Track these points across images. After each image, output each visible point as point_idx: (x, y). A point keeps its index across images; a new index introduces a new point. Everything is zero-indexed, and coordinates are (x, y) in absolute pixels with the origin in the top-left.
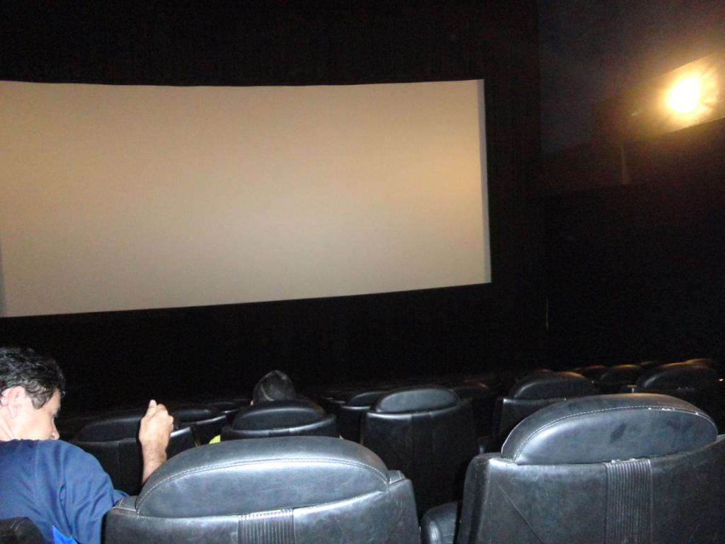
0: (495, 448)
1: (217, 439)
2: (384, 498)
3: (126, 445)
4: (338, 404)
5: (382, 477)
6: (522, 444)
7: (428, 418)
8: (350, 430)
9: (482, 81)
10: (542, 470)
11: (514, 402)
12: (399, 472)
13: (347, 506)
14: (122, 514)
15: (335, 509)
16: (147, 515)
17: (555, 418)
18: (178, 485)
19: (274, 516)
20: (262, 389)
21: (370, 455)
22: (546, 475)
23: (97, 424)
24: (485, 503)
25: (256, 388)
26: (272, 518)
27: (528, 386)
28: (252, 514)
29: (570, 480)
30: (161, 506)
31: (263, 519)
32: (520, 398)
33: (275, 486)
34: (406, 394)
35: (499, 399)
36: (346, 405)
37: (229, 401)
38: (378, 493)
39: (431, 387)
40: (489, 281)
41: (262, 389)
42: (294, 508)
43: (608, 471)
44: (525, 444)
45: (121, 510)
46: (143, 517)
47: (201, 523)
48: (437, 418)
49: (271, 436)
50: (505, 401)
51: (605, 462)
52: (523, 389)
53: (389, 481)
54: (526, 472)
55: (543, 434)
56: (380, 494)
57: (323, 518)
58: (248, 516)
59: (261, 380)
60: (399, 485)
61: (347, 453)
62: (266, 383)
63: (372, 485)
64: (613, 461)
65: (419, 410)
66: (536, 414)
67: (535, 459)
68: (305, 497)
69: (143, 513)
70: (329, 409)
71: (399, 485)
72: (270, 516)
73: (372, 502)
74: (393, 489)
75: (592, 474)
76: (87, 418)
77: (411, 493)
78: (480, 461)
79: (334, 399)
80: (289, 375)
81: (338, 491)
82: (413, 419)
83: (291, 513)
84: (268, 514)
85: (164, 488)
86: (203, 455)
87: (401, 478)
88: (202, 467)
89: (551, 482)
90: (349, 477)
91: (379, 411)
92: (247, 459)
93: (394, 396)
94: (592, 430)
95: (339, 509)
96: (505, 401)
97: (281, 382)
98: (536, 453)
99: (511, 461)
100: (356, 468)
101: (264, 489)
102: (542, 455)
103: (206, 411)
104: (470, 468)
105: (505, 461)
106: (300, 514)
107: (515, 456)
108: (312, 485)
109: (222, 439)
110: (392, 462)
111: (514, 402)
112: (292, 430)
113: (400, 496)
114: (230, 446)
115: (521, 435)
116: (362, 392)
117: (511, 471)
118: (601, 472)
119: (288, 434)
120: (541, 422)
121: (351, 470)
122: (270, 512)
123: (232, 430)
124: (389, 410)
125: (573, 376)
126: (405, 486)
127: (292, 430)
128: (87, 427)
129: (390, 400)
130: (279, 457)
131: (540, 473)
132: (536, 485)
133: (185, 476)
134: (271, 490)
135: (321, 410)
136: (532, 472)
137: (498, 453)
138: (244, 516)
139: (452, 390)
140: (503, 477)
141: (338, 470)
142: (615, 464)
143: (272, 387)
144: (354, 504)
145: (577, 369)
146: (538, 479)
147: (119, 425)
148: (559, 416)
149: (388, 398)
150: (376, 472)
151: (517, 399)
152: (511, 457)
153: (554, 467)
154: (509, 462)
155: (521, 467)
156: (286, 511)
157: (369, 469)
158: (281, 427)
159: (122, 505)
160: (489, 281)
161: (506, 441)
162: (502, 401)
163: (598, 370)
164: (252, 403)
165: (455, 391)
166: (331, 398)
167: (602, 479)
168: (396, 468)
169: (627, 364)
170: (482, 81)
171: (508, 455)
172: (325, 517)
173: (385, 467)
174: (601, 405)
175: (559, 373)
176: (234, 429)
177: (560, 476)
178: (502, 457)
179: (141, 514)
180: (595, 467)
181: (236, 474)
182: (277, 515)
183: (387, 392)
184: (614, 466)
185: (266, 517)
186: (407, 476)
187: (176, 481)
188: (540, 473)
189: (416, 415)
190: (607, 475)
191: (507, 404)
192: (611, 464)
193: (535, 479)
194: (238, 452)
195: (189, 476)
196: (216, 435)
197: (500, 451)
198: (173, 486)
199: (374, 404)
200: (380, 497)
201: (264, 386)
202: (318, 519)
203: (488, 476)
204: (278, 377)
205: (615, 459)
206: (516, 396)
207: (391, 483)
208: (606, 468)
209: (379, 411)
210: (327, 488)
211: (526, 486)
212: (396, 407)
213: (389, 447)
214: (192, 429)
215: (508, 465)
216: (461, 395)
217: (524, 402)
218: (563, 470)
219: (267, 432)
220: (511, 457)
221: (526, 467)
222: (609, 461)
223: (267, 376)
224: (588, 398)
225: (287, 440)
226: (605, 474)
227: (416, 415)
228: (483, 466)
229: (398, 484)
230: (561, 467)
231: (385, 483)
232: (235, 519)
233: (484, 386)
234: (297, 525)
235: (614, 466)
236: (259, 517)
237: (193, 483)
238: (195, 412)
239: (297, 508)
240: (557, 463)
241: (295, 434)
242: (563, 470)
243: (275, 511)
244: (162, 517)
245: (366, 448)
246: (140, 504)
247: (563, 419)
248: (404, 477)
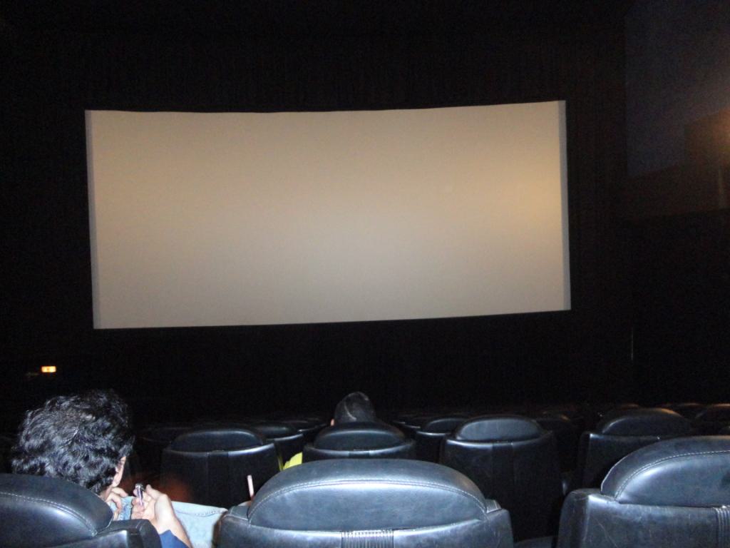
0: (595, 485)
1: (297, 460)
2: (481, 527)
3: (214, 456)
4: (412, 430)
5: (480, 506)
6: (625, 482)
7: (510, 448)
8: (430, 455)
9: (563, 103)
10: (646, 510)
11: (602, 437)
12: (494, 501)
13: (446, 531)
14: (235, 522)
15: (434, 533)
16: (258, 525)
17: (660, 457)
18: (288, 499)
19: (375, 535)
20: (346, 408)
21: (467, 482)
22: (650, 516)
23: (189, 435)
24: (584, 539)
25: (339, 405)
26: (373, 538)
27: (617, 422)
28: (354, 532)
29: (676, 522)
30: (270, 516)
31: (365, 538)
32: (608, 434)
33: (376, 507)
34: (486, 422)
35: (587, 433)
36: (421, 430)
37: (302, 419)
38: (476, 521)
39: (506, 417)
40: (87, 112)
41: (346, 408)
42: (393, 530)
43: (719, 516)
44: (627, 482)
45: (234, 519)
46: (254, 526)
47: (307, 536)
48: (520, 450)
49: (351, 457)
50: (592, 435)
51: (715, 507)
52: (612, 424)
53: (486, 510)
54: (629, 511)
55: (646, 474)
56: (478, 523)
57: (421, 541)
58: (350, 533)
59: (345, 398)
60: (497, 514)
61: (447, 479)
62: (349, 402)
63: (470, 513)
64: (724, 507)
65: (501, 440)
66: (640, 451)
67: (639, 498)
68: (407, 518)
69: (254, 522)
70: (410, 435)
71: (497, 514)
72: (371, 535)
73: (470, 529)
74: (491, 518)
75: (702, 518)
76: (180, 428)
77: (507, 524)
78: (577, 497)
79: (407, 423)
80: (370, 398)
81: (437, 517)
82: (494, 448)
83: (391, 534)
84: (373, 533)
85: (275, 500)
86: (310, 471)
87: (497, 509)
88: (310, 483)
89: (655, 523)
90: (449, 503)
91: (459, 438)
92: (352, 478)
93: (475, 424)
94: (702, 472)
95: (332, 539)
96: (592, 435)
97: (362, 404)
98: (634, 489)
99: (612, 498)
100: (456, 495)
101: (366, 509)
102: (646, 495)
103: (284, 429)
104: (566, 505)
105: (606, 498)
106: (399, 535)
107: (617, 493)
108: (413, 508)
109: (305, 460)
110: (489, 490)
111: (602, 437)
112: (371, 452)
113: (497, 525)
114: (335, 465)
115: (622, 473)
116: (436, 419)
117: (612, 509)
118: (710, 517)
119: (368, 456)
120: (644, 461)
121: (451, 496)
122: (371, 531)
123: (313, 449)
124: (470, 438)
125: (667, 414)
126: (502, 517)
127: (371, 452)
128: (180, 438)
129: (470, 428)
130: (382, 479)
131: (643, 513)
132: (639, 526)
133: (295, 491)
134: (373, 510)
135: (400, 434)
136: (635, 511)
137: (598, 490)
138: (347, 533)
139: (534, 421)
140: (604, 516)
141: (439, 495)
142: (725, 510)
143: (354, 406)
144: (452, 531)
145: (668, 405)
146: (641, 519)
147: (209, 437)
148: (664, 455)
149: (467, 427)
150: (475, 500)
151: (604, 434)
152: (613, 495)
153: (658, 508)
154: (610, 500)
155: (622, 505)
156: (387, 532)
157: (468, 496)
158: (361, 449)
159: (233, 513)
160: (87, 112)
161: (606, 478)
162: (589, 436)
163: (691, 408)
164: (332, 423)
165: (538, 422)
166: (404, 423)
167: (712, 525)
168: (492, 497)
169: (723, 402)
170: (563, 103)
171: (609, 492)
172: (424, 541)
173: (481, 495)
174: (711, 446)
175: (650, 410)
176: (316, 448)
177: (664, 518)
178: (602, 494)
179: (252, 523)
180: (703, 511)
181: (341, 492)
182: (378, 535)
183: (466, 421)
184: (725, 512)
185: (368, 535)
186: (503, 506)
187: (286, 494)
188: (643, 513)
189: (497, 445)
190: (717, 519)
191: (593, 439)
192: (722, 509)
193: (639, 519)
194: (323, 474)
195: (298, 490)
196: (297, 452)
197: (599, 487)
198: (283, 499)
199: (453, 433)
200: (478, 525)
201: (347, 405)
202: (417, 542)
203: (588, 512)
204: (361, 398)
205: (726, 505)
206: (604, 432)
207: (488, 512)
208: (716, 513)
209: (459, 438)
210: (426, 512)
211: (628, 526)
212: (475, 435)
213: (488, 475)
214: (275, 445)
215: (610, 502)
216: (543, 425)
217: (610, 438)
218: (669, 512)
219: (347, 453)
220: (613, 495)
221: (628, 506)
222: (719, 507)
223: (350, 395)
224: (697, 438)
225: (387, 462)
226: (715, 519)
227: (497, 445)
228: (583, 502)
229: (494, 512)
230: (666, 509)
231: (483, 511)
232: (337, 535)
233: (565, 418)
234: (397, 544)
235: (725, 512)
236: (361, 536)
237: (302, 497)
238: (274, 429)
239: (397, 529)
240: (661, 504)
241: (375, 457)
242: (669, 512)
243: (376, 531)
244: (271, 527)
245: (460, 473)
246: (252, 514)
247: (669, 458)
248: (500, 508)
